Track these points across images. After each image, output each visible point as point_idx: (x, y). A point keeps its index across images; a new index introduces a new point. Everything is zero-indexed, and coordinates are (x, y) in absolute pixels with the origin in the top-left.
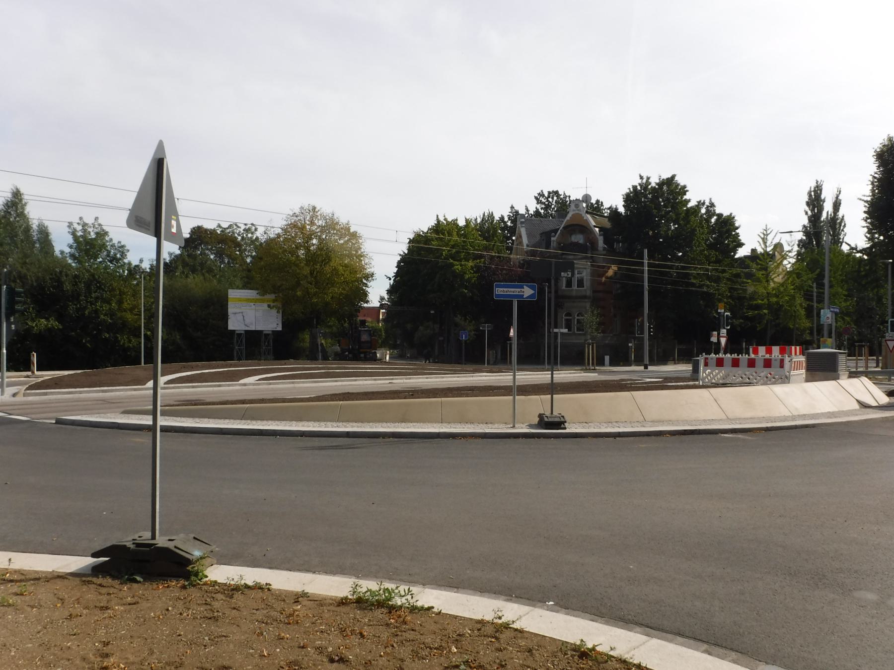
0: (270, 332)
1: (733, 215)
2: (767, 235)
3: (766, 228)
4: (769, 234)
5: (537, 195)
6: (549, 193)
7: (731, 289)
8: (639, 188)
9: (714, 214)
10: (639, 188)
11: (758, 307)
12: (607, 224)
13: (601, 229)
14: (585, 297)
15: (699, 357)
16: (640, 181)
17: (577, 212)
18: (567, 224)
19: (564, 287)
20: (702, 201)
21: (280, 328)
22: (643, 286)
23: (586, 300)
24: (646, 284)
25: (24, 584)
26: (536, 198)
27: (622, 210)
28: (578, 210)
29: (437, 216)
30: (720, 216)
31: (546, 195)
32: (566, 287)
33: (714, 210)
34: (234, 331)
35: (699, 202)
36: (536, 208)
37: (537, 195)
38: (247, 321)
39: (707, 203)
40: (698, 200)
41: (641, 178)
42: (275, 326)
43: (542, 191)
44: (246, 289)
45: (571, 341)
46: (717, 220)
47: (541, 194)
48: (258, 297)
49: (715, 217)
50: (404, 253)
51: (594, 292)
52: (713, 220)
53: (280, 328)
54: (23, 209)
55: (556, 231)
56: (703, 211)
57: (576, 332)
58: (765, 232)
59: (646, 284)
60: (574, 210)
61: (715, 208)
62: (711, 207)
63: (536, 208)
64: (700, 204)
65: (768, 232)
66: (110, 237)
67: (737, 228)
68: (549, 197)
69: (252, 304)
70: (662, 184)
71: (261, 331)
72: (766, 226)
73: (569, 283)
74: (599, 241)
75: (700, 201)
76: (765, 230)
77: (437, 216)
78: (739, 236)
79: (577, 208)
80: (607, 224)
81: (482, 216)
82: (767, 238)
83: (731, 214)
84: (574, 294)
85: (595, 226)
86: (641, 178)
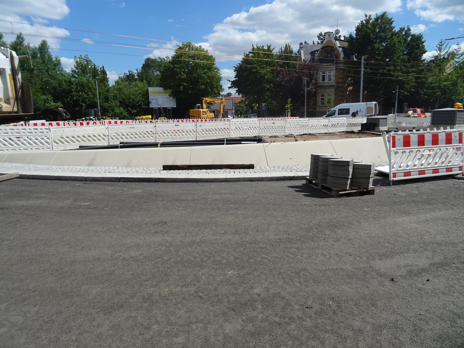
0: (171, 108)
1: (421, 34)
2: (442, 45)
3: (442, 41)
4: (443, 44)
5: (318, 35)
6: (325, 33)
7: (417, 78)
8: (364, 22)
9: (410, 35)
10: (364, 22)
11: (433, 88)
12: (346, 44)
13: (343, 48)
14: (332, 86)
15: (446, 129)
16: (365, 18)
17: (329, 39)
18: (325, 46)
19: (321, 81)
20: (403, 28)
21: (175, 106)
22: (360, 77)
23: (333, 88)
24: (362, 76)
25: (412, 224)
26: (318, 36)
27: (354, 36)
28: (330, 38)
29: (253, 45)
30: (413, 36)
31: (323, 35)
32: (322, 81)
33: (410, 33)
34: (153, 108)
35: (401, 29)
36: (318, 42)
37: (318, 35)
38: (159, 103)
39: (406, 29)
40: (401, 27)
41: (366, 16)
42: (173, 105)
43: (321, 32)
44: (158, 87)
45: (324, 110)
46: (411, 39)
47: (321, 34)
48: (163, 91)
49: (410, 37)
50: (237, 66)
51: (337, 83)
52: (409, 39)
53: (175, 106)
54: (48, 50)
55: (317, 51)
56: (404, 33)
57: (320, 105)
58: (440, 44)
59: (362, 76)
60: (328, 38)
61: (411, 31)
62: (408, 31)
63: (318, 42)
64: (402, 30)
65: (443, 43)
66: (8, 44)
67: (423, 42)
68: (325, 35)
69: (161, 94)
70: (377, 19)
71: (166, 108)
72: (442, 40)
73: (324, 79)
74: (341, 55)
75: (402, 28)
76: (440, 42)
77: (253, 45)
78: (424, 47)
79: (329, 37)
80: (346, 44)
81: (285, 47)
82: (441, 48)
83: (420, 34)
84: (326, 84)
85: (339, 47)
86: (366, 16)
